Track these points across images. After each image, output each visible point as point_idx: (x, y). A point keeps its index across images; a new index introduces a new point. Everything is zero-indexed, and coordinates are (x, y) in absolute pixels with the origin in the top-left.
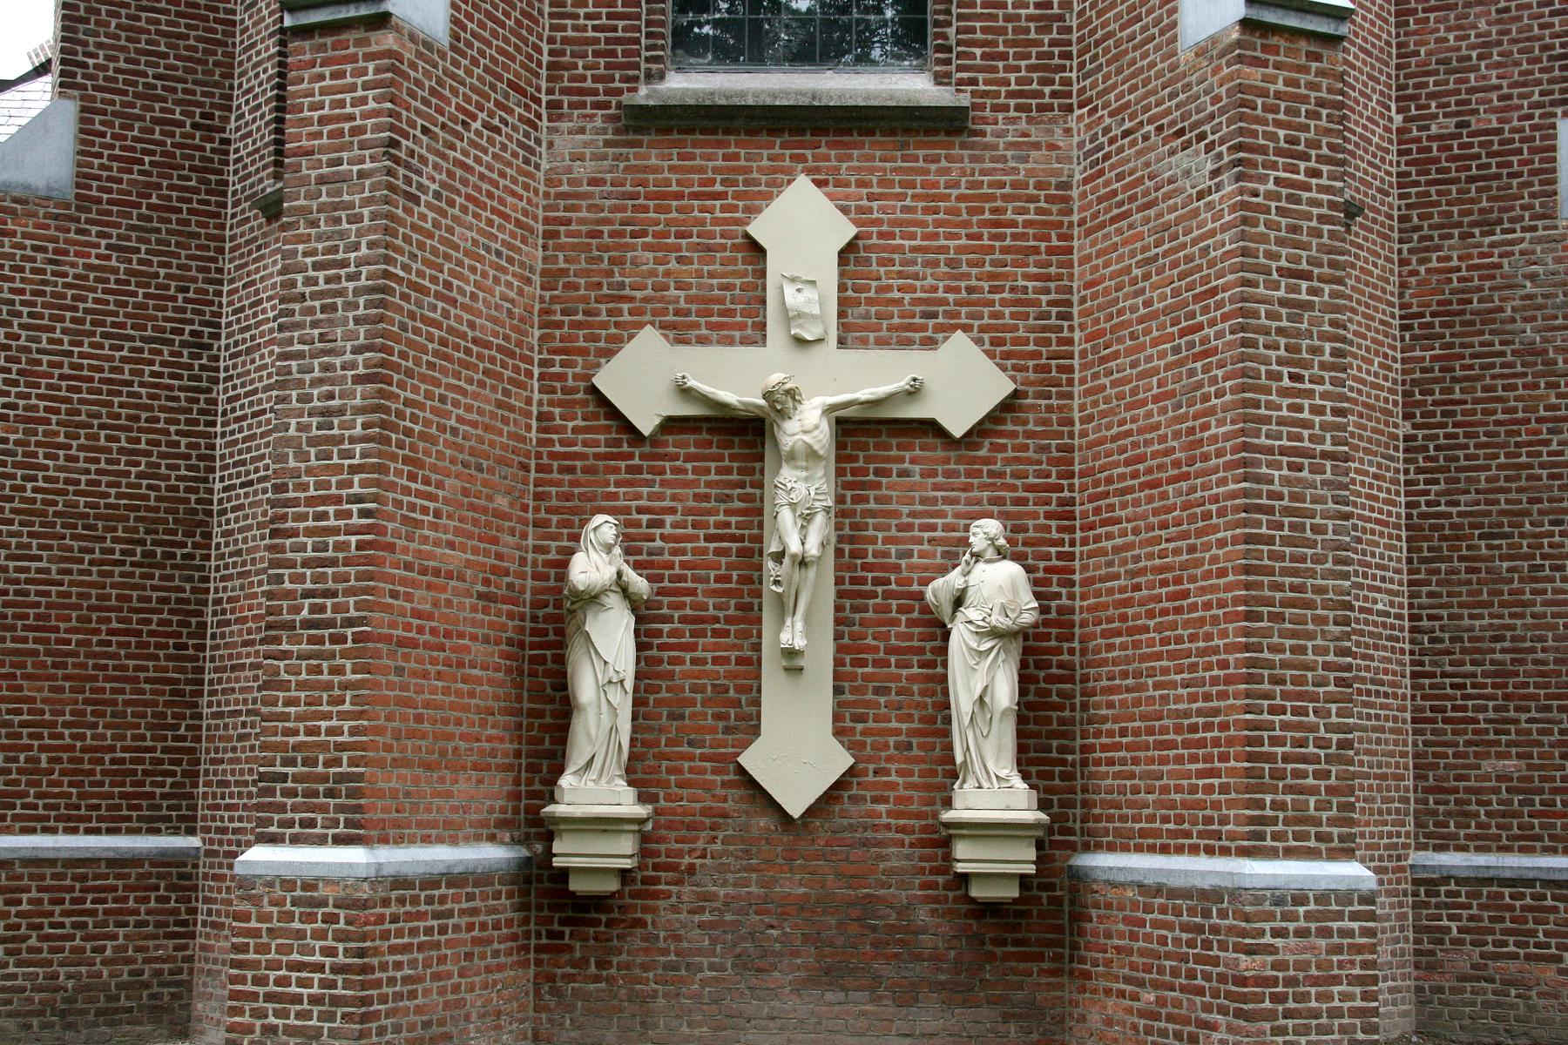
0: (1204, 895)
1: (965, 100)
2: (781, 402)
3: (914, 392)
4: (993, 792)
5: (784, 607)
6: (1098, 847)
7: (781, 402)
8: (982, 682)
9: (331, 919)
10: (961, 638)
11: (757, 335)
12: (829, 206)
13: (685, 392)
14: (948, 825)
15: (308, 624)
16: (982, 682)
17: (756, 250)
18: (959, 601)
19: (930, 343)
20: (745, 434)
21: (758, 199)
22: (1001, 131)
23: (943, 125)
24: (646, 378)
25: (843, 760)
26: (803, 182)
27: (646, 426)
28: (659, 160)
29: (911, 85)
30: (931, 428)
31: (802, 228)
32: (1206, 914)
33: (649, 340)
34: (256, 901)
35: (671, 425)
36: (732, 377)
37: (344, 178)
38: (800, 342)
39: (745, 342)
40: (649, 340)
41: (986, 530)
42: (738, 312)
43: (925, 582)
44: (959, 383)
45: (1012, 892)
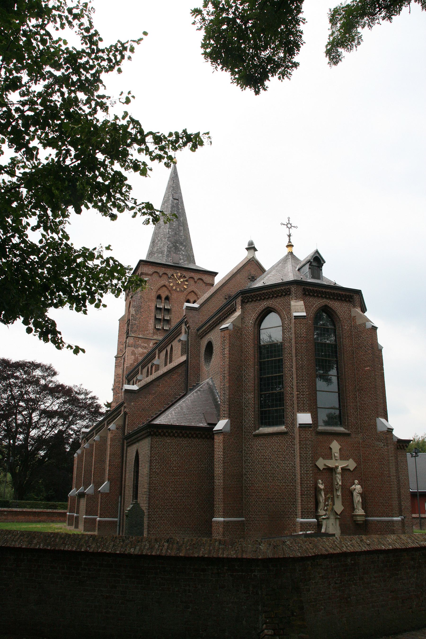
0: (387, 521)
1: (350, 432)
2: (337, 467)
3: (347, 466)
4: (360, 511)
5: (337, 490)
6: (369, 517)
7: (337, 467)
8: (357, 499)
9: (313, 527)
10: (355, 493)
11: (331, 459)
12: (338, 444)
13: (325, 465)
14: (353, 515)
15: (306, 494)
16: (357, 499)
17: (331, 449)
18: (355, 489)
19: (348, 460)
20: (331, 470)
21: (331, 442)
22: (353, 435)
23: (348, 435)
24: (321, 463)
25: (343, 508)
26: (335, 441)
27: (321, 469)
28: (320, 437)
29: (341, 429)
30: (349, 470)
31: (335, 446)
32: (388, 523)
33: (321, 459)
34: (303, 525)
35: (324, 469)
36: (331, 464)
37: (307, 444)
38: (336, 460)
39: (330, 459)
40: (321, 459)
41: (356, 481)
42: (329, 455)
43: (350, 487)
44: (351, 464)
45: (362, 522)
